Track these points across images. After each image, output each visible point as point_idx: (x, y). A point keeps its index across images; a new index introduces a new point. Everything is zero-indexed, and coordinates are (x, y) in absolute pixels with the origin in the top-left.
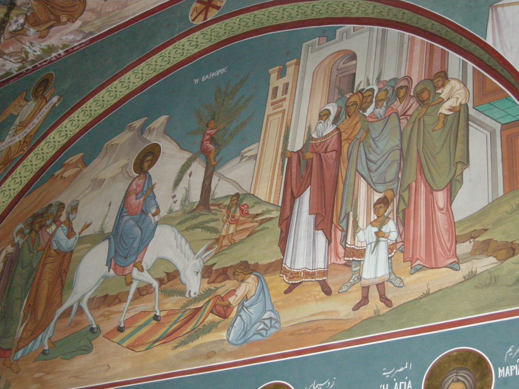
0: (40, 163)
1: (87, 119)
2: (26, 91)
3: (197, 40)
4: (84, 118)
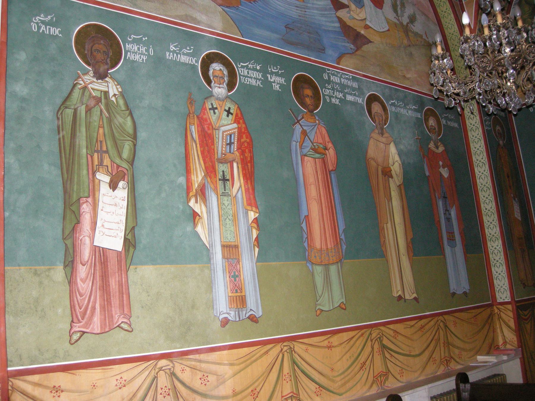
0: (502, 268)
1: (502, 268)
3: (444, 12)
4: (490, 206)
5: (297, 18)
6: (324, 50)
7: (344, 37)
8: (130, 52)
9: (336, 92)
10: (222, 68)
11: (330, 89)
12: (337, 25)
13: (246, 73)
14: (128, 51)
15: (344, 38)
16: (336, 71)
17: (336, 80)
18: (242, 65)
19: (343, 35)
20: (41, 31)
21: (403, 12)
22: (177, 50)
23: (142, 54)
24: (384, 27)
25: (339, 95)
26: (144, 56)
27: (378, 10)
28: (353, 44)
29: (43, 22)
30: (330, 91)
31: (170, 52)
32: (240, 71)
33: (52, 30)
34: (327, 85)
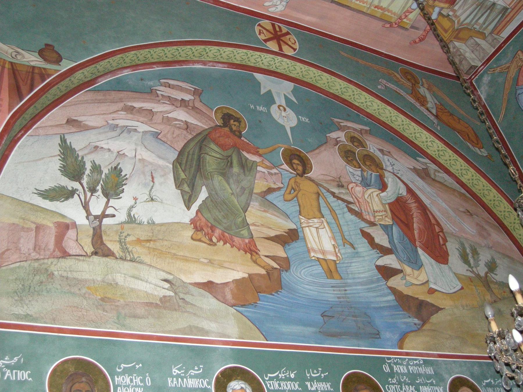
5: (336, 302)
6: (378, 334)
7: (404, 311)
8: (121, 386)
9: (405, 386)
10: (243, 386)
11: (395, 384)
12: (391, 297)
13: (277, 385)
14: (119, 385)
15: (403, 312)
16: (400, 359)
17: (402, 370)
18: (269, 377)
19: (401, 309)
20: (5, 378)
21: (477, 260)
22: (182, 373)
23: (136, 386)
24: (455, 286)
25: (409, 388)
26: (140, 388)
27: (443, 266)
28: (416, 317)
29: (8, 366)
30: (395, 387)
31: (173, 377)
32: (268, 385)
33: (20, 374)
34: (390, 379)
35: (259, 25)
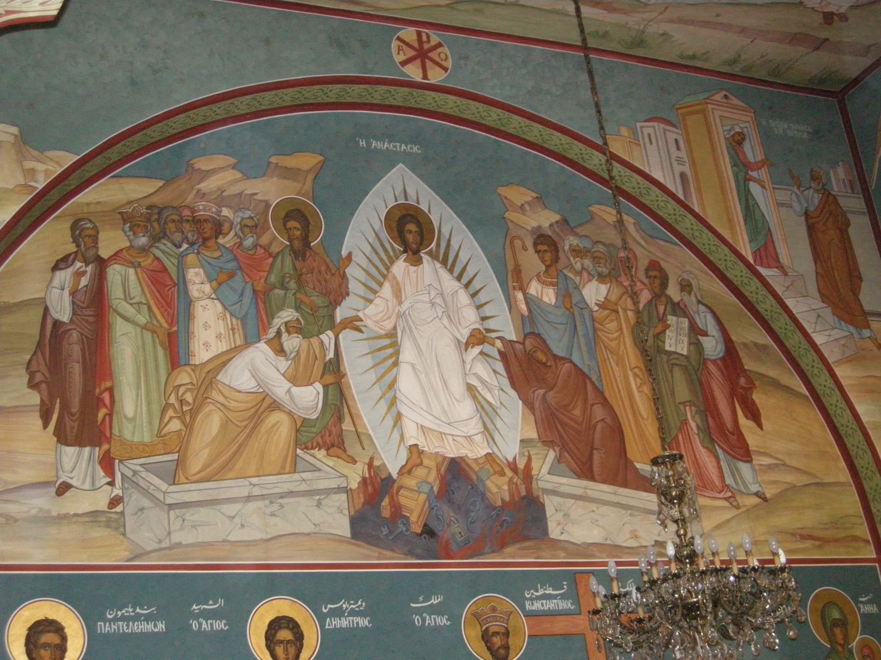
2: (565, 221)
35: (399, 39)
